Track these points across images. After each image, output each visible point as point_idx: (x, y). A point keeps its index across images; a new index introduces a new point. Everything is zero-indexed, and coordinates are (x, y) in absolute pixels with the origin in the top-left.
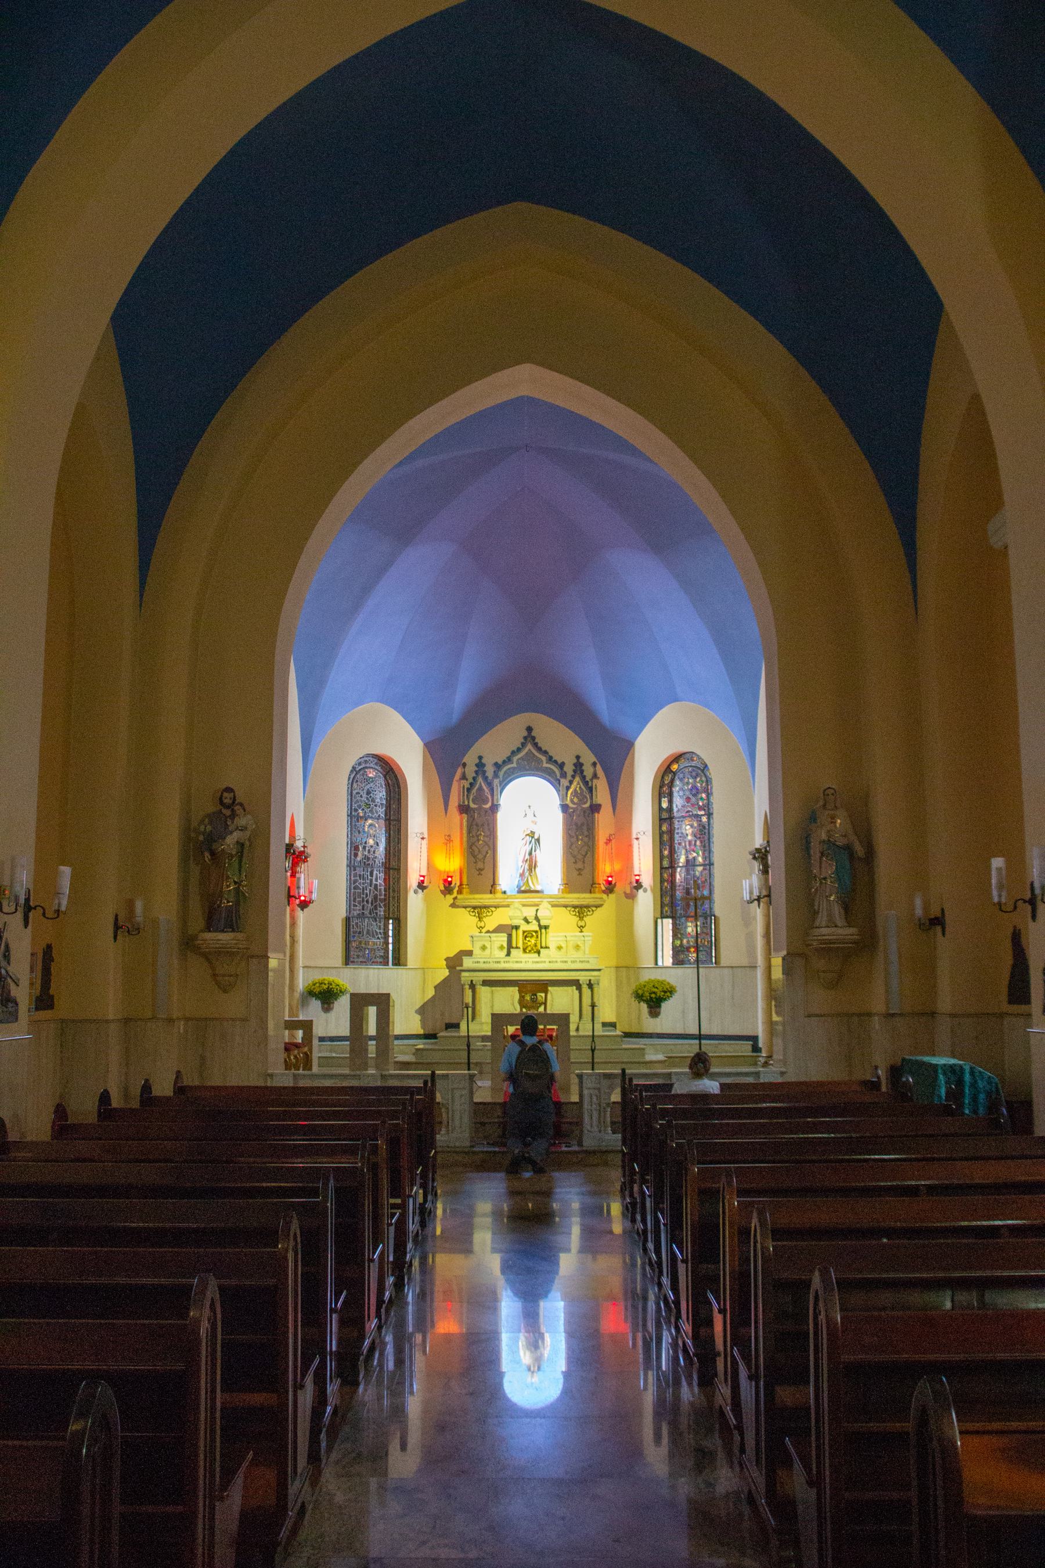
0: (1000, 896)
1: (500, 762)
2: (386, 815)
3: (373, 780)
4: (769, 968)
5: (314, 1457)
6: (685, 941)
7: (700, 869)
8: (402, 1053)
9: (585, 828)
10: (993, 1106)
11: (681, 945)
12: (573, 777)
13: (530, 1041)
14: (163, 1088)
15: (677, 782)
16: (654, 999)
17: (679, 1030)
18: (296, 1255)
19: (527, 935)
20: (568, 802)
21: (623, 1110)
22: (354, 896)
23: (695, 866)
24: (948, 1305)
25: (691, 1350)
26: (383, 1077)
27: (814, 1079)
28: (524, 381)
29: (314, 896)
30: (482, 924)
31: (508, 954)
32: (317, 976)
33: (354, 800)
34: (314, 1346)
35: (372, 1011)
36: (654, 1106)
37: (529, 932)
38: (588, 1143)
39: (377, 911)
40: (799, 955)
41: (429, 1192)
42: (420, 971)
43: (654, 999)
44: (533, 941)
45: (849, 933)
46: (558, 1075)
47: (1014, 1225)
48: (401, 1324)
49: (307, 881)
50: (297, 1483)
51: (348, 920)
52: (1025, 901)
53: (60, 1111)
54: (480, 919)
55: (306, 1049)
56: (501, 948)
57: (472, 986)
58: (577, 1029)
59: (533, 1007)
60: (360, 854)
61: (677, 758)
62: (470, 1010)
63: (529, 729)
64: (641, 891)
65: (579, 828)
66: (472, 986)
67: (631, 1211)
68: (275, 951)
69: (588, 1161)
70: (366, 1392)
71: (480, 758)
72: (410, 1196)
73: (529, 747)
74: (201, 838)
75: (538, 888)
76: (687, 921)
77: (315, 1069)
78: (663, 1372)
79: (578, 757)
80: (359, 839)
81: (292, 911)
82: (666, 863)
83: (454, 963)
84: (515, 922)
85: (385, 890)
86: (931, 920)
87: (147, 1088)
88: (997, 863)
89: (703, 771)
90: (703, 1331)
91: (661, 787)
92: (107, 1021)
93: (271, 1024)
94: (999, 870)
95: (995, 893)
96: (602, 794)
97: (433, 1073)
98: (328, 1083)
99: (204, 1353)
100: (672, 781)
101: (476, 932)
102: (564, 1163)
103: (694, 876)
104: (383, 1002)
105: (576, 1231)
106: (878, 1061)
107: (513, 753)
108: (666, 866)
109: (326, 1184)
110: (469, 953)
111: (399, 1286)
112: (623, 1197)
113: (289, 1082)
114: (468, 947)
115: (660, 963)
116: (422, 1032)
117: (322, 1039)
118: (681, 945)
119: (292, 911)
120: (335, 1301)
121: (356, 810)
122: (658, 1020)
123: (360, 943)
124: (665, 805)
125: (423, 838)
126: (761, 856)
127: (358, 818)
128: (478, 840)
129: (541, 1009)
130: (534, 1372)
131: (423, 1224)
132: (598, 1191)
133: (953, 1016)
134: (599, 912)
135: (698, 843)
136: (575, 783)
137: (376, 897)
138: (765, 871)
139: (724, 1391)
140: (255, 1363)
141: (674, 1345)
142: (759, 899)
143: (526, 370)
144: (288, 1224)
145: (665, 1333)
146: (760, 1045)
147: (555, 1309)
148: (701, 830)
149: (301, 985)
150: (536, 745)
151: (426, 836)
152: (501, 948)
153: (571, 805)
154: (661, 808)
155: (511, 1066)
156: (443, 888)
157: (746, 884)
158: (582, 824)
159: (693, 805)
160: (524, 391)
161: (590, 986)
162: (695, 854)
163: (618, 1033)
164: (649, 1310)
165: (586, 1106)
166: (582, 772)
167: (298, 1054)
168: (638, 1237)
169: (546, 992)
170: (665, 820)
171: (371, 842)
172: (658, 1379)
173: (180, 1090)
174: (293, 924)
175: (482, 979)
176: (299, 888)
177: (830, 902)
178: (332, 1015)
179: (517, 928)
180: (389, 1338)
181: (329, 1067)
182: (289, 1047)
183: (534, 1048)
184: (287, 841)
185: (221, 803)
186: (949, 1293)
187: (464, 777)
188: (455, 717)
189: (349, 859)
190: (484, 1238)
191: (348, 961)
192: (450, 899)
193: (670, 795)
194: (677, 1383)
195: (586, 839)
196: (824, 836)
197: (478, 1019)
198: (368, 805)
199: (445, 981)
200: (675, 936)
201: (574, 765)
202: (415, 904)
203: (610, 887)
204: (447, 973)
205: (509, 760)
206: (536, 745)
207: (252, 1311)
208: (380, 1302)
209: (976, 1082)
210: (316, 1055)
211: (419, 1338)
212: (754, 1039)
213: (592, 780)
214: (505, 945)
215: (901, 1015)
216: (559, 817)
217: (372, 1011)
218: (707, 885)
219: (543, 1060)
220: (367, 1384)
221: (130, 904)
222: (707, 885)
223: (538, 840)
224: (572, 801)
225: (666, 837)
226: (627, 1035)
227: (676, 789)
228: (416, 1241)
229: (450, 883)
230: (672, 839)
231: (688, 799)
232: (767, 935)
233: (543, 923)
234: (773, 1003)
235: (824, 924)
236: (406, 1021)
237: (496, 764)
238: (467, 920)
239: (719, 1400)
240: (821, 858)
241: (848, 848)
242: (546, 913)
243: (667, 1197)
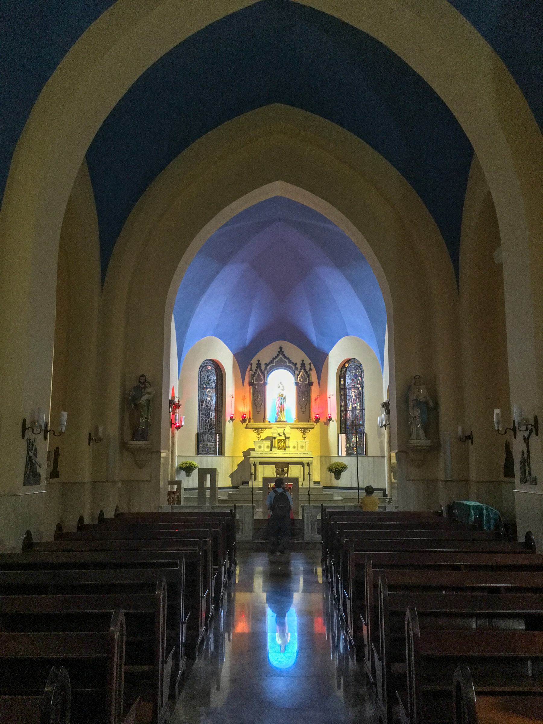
0: (498, 427)
3: (210, 371)
4: (390, 458)
5: (172, 697)
7: (358, 411)
8: (222, 496)
9: (306, 392)
10: (497, 527)
11: (350, 446)
12: (301, 369)
13: (280, 490)
14: (110, 514)
15: (348, 372)
16: (337, 471)
17: (349, 486)
18: (165, 596)
19: (279, 441)
20: (298, 381)
21: (322, 523)
22: (202, 423)
23: (356, 410)
24: (474, 626)
25: (353, 643)
26: (213, 507)
27: (412, 510)
28: (278, 189)
31: (271, 450)
32: (184, 460)
34: (173, 641)
35: (208, 476)
36: (335, 522)
37: (281, 440)
38: (307, 538)
40: (403, 452)
41: (233, 563)
42: (231, 458)
43: (337, 471)
44: (282, 444)
45: (428, 442)
46: (292, 507)
47: (507, 587)
48: (217, 628)
49: (180, 417)
50: (163, 710)
51: (198, 435)
52: (510, 429)
53: (59, 527)
55: (178, 494)
56: (268, 447)
57: (255, 465)
58: (302, 485)
59: (282, 474)
61: (348, 361)
62: (253, 476)
63: (281, 348)
64: (331, 421)
65: (303, 392)
66: (255, 465)
67: (326, 572)
68: (164, 449)
69: (306, 548)
70: (199, 663)
71: (259, 361)
72: (223, 565)
73: (281, 356)
74: (130, 398)
75: (285, 420)
77: (182, 503)
78: (341, 653)
79: (303, 361)
81: (173, 430)
82: (343, 409)
83: (247, 454)
84: (274, 435)
86: (466, 437)
87: (102, 514)
88: (497, 411)
89: (359, 367)
90: (358, 634)
91: (341, 374)
92: (84, 483)
93: (162, 483)
94: (498, 414)
95: (496, 425)
96: (314, 378)
97: (235, 506)
98: (187, 511)
99: (116, 646)
100: (346, 371)
101: (256, 440)
102: (295, 548)
103: (356, 415)
104: (213, 472)
105: (301, 580)
106: (443, 499)
107: (274, 359)
109: (181, 562)
110: (253, 450)
111: (217, 609)
112: (323, 566)
113: (169, 511)
114: (253, 447)
115: (340, 455)
116: (231, 486)
117: (185, 489)
118: (350, 446)
119: (173, 430)
120: (183, 618)
121: (202, 385)
122: (339, 481)
124: (342, 382)
126: (386, 406)
127: (203, 388)
129: (286, 475)
130: (283, 648)
131: (229, 578)
132: (311, 563)
133: (446, 481)
136: (301, 372)
137: (211, 423)
138: (388, 413)
139: (368, 664)
140: (142, 651)
141: (345, 640)
142: (385, 426)
143: (279, 184)
144: (161, 582)
145: (342, 634)
146: (387, 493)
147: (293, 618)
148: (358, 394)
149: (176, 464)
150: (284, 355)
151: (234, 396)
152: (268, 447)
153: (300, 382)
155: (271, 502)
157: (379, 419)
158: (305, 391)
159: (355, 382)
160: (278, 193)
161: (308, 464)
163: (321, 486)
164: (334, 622)
165: (306, 521)
167: (174, 497)
168: (329, 585)
169: (288, 468)
170: (342, 390)
171: (209, 399)
172: (339, 656)
173: (118, 515)
174: (173, 436)
176: (176, 420)
177: (418, 427)
178: (191, 478)
179: (275, 438)
180: (211, 635)
181: (187, 504)
182: (170, 493)
183: (281, 494)
184: (170, 398)
185: (140, 381)
186: (474, 619)
187: (251, 370)
188: (247, 342)
189: (199, 406)
190: (259, 583)
191: (198, 453)
194: (347, 659)
195: (306, 398)
196: (415, 398)
197: (257, 480)
198: (208, 382)
200: (347, 442)
202: (229, 427)
203: (317, 420)
205: (272, 362)
206: (284, 355)
207: (142, 625)
208: (207, 617)
209: (489, 514)
210: (183, 496)
211: (226, 635)
212: (384, 490)
214: (270, 446)
215: (452, 481)
216: (294, 388)
217: (208, 476)
218: (362, 419)
219: (286, 499)
220: (199, 659)
221: (97, 428)
222: (362, 419)
223: (285, 398)
225: (342, 397)
226: (325, 487)
227: (347, 375)
228: (225, 587)
229: (245, 417)
230: (345, 398)
231: (353, 380)
232: (390, 442)
233: (287, 436)
234: (392, 474)
235: (415, 438)
236: (224, 481)
238: (252, 435)
239: (366, 669)
240: (413, 407)
241: (426, 403)
242: (288, 430)
243: (342, 566)
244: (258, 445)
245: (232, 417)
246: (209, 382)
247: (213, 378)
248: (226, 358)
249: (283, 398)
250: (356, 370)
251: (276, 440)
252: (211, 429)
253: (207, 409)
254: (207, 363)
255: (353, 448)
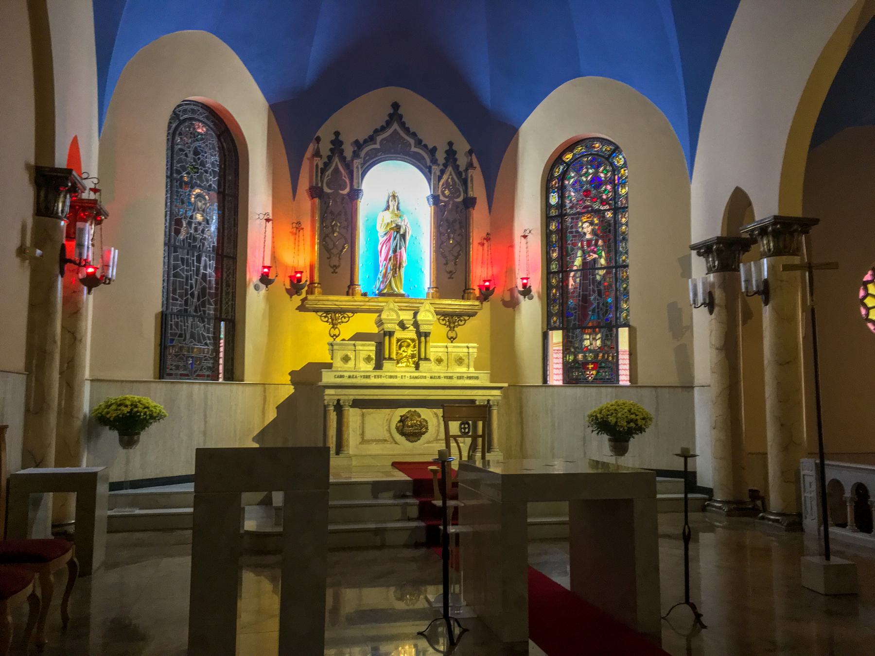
1: (361, 142)
2: (219, 186)
6: (580, 356)
7: (602, 272)
9: (457, 226)
11: (575, 361)
22: (175, 284)
29: (112, 272)
30: (336, 332)
32: (114, 394)
33: (176, 158)
39: (201, 321)
42: (259, 389)
51: (163, 319)
54: (334, 326)
56: (368, 359)
60: (183, 231)
61: (570, 146)
63: (396, 106)
65: (450, 224)
66: (339, 407)
71: (337, 134)
73: (396, 126)
75: (402, 292)
76: (583, 333)
79: (450, 144)
80: (182, 211)
82: (554, 267)
84: (388, 327)
85: (217, 283)
89: (607, 159)
96: (478, 189)
107: (377, 132)
108: (556, 268)
110: (329, 366)
118: (575, 361)
121: (179, 172)
123: (181, 348)
125: (268, 220)
128: (333, 232)
134: (472, 322)
135: (600, 242)
137: (203, 289)
149: (86, 404)
150: (403, 125)
152: (368, 359)
153: (442, 198)
154: (547, 206)
156: (288, 287)
158: (455, 221)
162: (595, 256)
166: (456, 160)
171: (199, 217)
175: (352, 398)
179: (391, 334)
187: (317, 154)
191: (162, 372)
192: (297, 300)
193: (562, 191)
195: (458, 239)
199: (290, 401)
201: (446, 152)
202: (255, 301)
203: (486, 294)
204: (291, 390)
205: (371, 139)
206: (403, 125)
212: (689, 478)
213: (466, 170)
223: (404, 236)
224: (443, 192)
225: (554, 238)
229: (299, 280)
230: (562, 239)
231: (587, 193)
233: (423, 328)
237: (357, 142)
238: (318, 326)
244: (339, 355)
245: (267, 274)
246: (198, 166)
247: (212, 159)
248: (251, 114)
249: (398, 233)
250: (598, 167)
251: (394, 340)
252: (203, 304)
253: (193, 246)
254: (193, 111)
255: (584, 364)
